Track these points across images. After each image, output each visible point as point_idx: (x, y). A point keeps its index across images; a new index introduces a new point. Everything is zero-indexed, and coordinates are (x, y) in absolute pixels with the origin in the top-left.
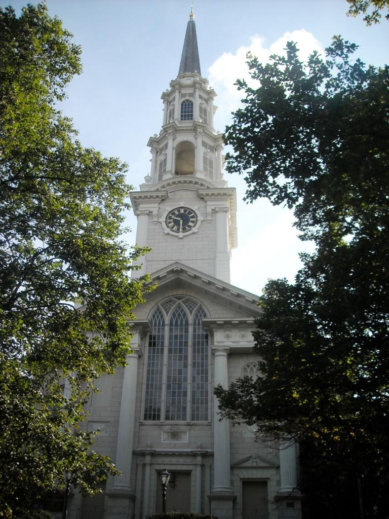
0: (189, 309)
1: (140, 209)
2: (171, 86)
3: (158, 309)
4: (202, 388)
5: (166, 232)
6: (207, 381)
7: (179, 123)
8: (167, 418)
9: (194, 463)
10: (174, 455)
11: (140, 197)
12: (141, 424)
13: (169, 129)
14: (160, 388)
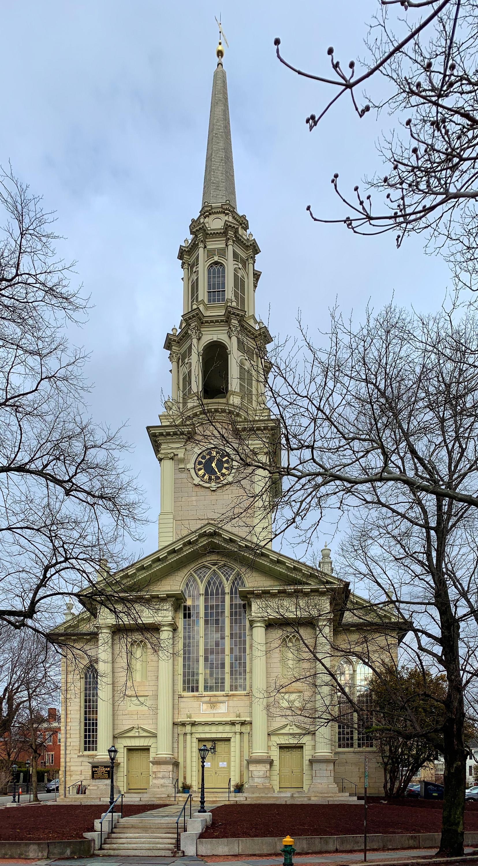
0: (225, 575)
1: (162, 452)
2: (192, 233)
3: (191, 575)
4: (240, 659)
5: (196, 482)
6: (245, 652)
7: (207, 308)
8: (206, 688)
9: (233, 731)
10: (213, 724)
11: (161, 434)
12: (181, 697)
13: (193, 319)
14: (198, 661)
